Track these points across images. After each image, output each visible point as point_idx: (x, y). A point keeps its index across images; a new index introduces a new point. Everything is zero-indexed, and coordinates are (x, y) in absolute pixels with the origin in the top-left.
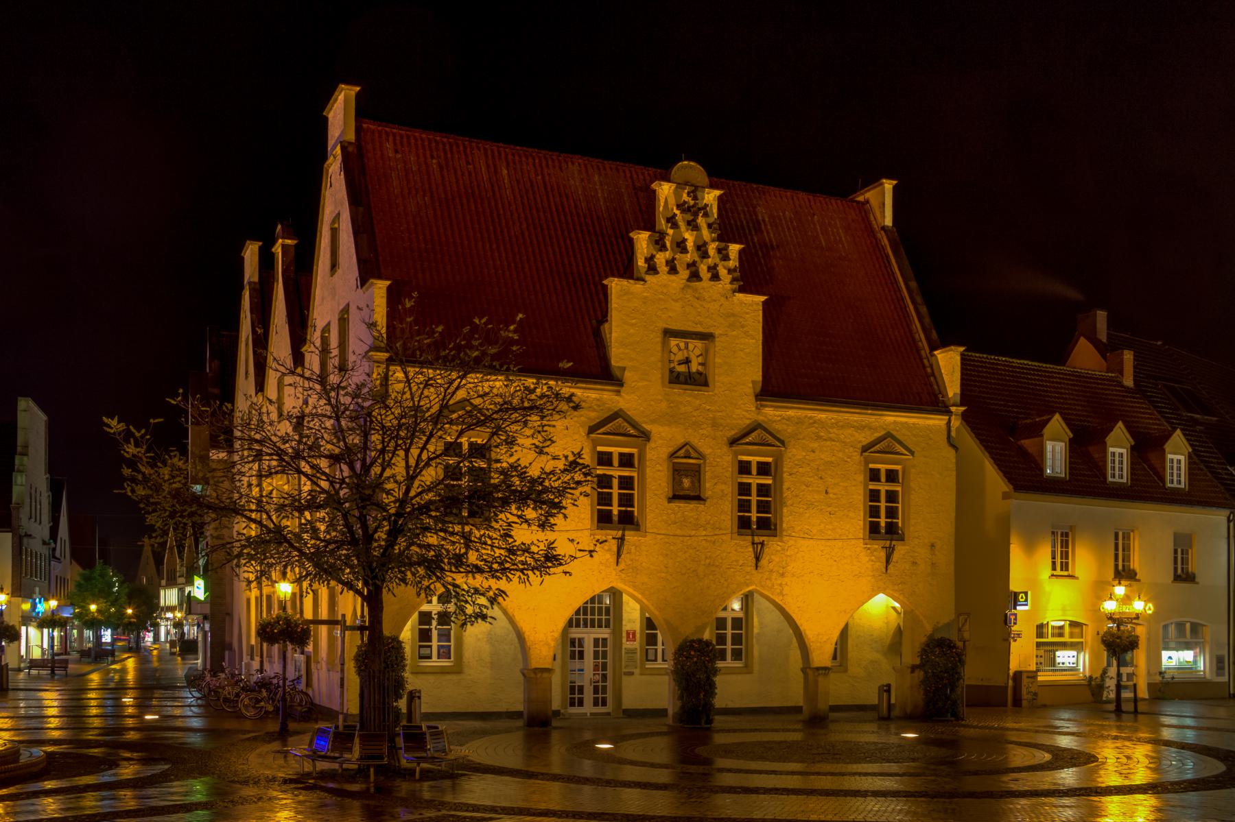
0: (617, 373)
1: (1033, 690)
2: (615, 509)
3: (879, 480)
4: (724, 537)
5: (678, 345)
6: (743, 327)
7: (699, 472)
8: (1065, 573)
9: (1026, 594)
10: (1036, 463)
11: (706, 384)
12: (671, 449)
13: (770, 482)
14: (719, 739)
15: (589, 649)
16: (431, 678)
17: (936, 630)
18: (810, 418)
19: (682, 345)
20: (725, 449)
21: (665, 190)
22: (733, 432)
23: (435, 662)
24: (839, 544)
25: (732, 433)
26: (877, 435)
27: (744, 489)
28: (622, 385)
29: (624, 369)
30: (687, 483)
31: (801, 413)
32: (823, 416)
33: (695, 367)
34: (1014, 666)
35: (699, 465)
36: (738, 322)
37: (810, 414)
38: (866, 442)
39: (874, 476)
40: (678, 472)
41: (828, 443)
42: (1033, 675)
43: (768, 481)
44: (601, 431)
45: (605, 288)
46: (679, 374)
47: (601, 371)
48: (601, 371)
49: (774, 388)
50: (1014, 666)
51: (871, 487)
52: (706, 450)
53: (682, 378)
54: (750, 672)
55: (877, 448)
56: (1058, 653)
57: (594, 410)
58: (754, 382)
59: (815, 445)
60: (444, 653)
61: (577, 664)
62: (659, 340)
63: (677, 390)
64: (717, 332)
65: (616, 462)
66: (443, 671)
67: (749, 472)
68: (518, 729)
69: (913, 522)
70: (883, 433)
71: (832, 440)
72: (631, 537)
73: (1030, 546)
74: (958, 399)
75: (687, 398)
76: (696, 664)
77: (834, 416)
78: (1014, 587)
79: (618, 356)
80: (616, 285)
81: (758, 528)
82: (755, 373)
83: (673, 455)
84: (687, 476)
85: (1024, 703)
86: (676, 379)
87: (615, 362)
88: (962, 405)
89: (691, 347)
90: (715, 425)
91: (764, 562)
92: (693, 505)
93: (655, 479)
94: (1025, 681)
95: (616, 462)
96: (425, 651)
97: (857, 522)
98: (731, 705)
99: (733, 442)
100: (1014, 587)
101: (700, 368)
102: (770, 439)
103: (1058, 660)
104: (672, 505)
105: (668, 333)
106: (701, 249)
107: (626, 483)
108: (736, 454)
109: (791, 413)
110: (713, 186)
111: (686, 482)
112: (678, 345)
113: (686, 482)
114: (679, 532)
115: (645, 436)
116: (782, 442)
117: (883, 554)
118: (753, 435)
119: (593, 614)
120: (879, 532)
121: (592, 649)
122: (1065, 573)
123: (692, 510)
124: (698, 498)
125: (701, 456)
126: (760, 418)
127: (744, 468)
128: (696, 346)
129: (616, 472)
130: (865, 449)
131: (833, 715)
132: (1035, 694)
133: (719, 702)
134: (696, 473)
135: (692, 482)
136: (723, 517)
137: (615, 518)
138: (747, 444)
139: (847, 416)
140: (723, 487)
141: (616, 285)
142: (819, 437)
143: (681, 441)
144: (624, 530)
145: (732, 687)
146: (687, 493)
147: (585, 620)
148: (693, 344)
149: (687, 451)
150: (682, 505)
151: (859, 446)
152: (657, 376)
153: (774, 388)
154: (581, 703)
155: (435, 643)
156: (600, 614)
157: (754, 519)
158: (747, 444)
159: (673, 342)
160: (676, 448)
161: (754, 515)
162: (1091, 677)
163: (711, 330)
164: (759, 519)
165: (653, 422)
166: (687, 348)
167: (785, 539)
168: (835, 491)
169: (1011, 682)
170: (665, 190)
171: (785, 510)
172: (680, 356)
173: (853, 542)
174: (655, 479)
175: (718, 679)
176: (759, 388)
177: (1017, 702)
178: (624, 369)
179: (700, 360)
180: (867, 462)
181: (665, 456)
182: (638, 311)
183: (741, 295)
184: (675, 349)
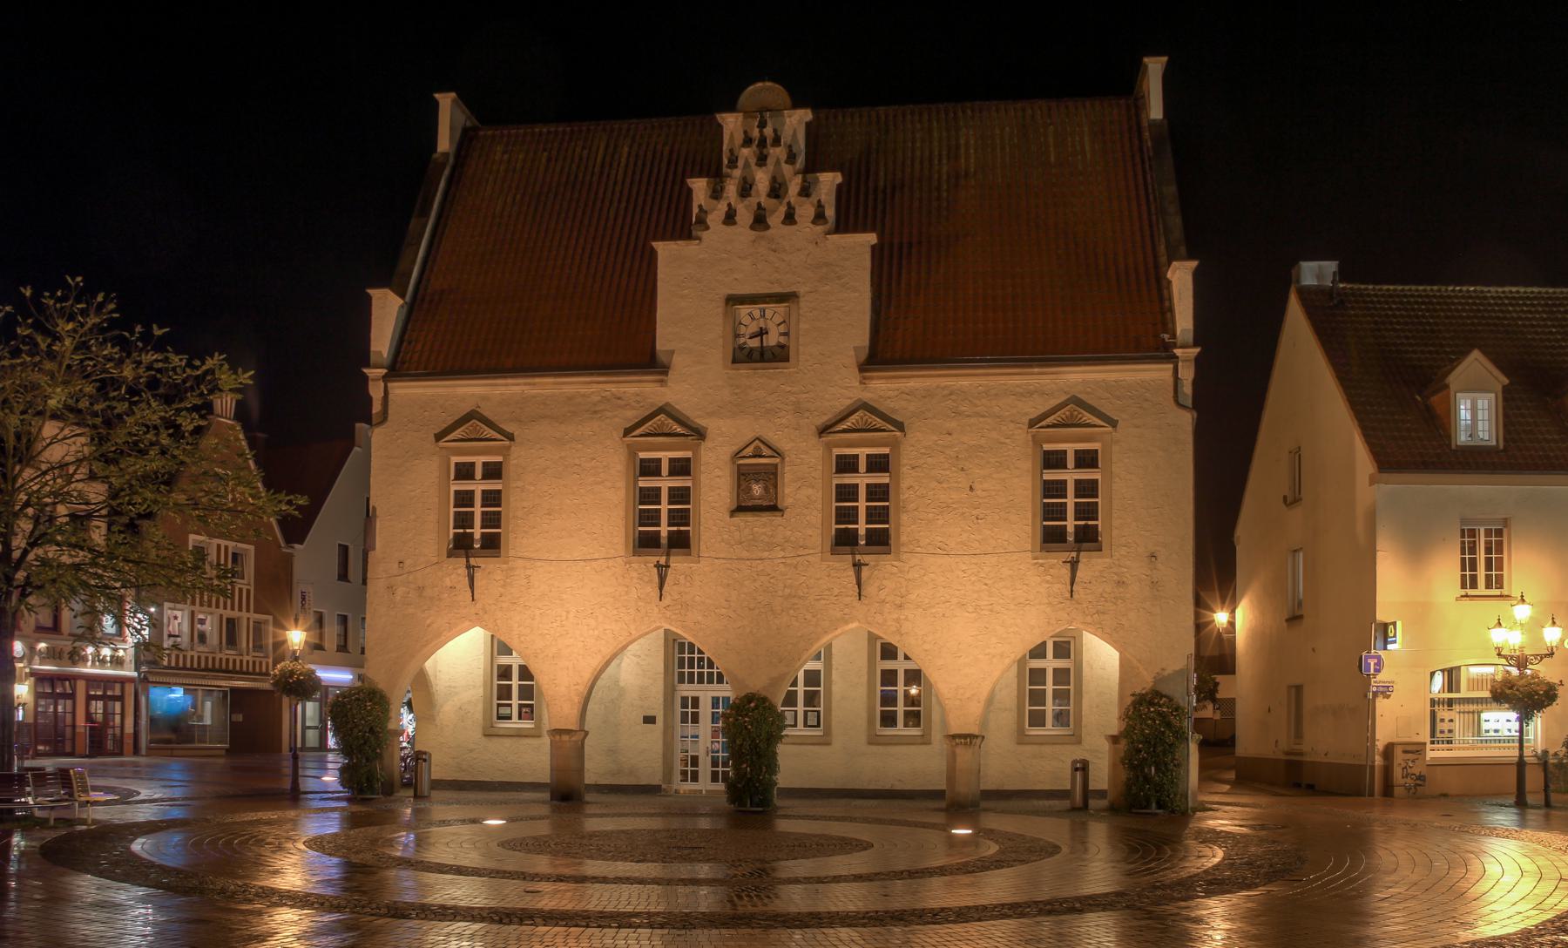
0: (662, 357)
1: (1416, 771)
2: (1071, 524)
3: (856, 471)
4: (810, 558)
5: (750, 314)
6: (839, 278)
7: (775, 474)
8: (1497, 592)
9: (1394, 624)
10: (1439, 423)
11: (787, 359)
12: (735, 448)
13: (887, 480)
14: (783, 825)
15: (705, 710)
16: (507, 742)
17: (1159, 680)
18: (944, 388)
19: (757, 314)
20: (814, 440)
21: (731, 123)
22: (825, 418)
23: (515, 724)
24: (994, 559)
25: (822, 420)
26: (1054, 402)
27: (846, 493)
28: (666, 373)
29: (673, 352)
30: (757, 489)
31: (929, 382)
32: (965, 383)
33: (772, 340)
34: (1385, 732)
35: (776, 466)
36: (834, 277)
37: (944, 382)
38: (1034, 414)
39: (1054, 460)
40: (744, 476)
41: (973, 420)
42: (1417, 749)
43: (883, 479)
44: (637, 432)
45: (653, 253)
46: (752, 349)
47: (649, 362)
48: (649, 362)
49: (881, 355)
50: (1385, 732)
51: (641, 484)
52: (783, 444)
53: (756, 355)
54: (928, 743)
55: (1050, 420)
56: (1484, 716)
57: (634, 408)
58: (856, 349)
59: (953, 425)
60: (1061, 718)
61: (690, 728)
62: (720, 310)
63: (744, 370)
64: (801, 290)
65: (1071, 461)
66: (519, 734)
67: (657, 473)
68: (544, 802)
69: (1115, 523)
70: (1064, 398)
71: (978, 415)
72: (678, 563)
73: (1417, 549)
74: (1190, 337)
75: (757, 379)
76: (752, 728)
77: (983, 381)
78: (1382, 616)
79: (666, 338)
80: (664, 249)
81: (867, 544)
82: (860, 336)
83: (737, 455)
84: (757, 481)
85: (1398, 791)
86: (744, 356)
87: (661, 345)
88: (1195, 345)
89: (769, 313)
90: (798, 410)
91: (869, 589)
92: (765, 518)
93: (714, 488)
94: (1399, 757)
95: (1071, 461)
96: (504, 711)
97: (1024, 525)
98: (899, 786)
99: (824, 430)
100: (1382, 616)
101: (782, 340)
102: (879, 423)
103: (1485, 726)
104: (736, 519)
105: (733, 300)
106: (777, 191)
107: (679, 495)
108: (829, 447)
109: (913, 384)
110: (796, 105)
111: (757, 489)
112: (750, 314)
113: (757, 489)
114: (745, 554)
115: (700, 434)
116: (900, 426)
117: (1065, 572)
118: (853, 419)
119: (691, 666)
120: (1065, 541)
121: (710, 710)
122: (1497, 592)
123: (764, 525)
124: (773, 508)
125: (778, 453)
126: (867, 396)
127: (846, 465)
128: (775, 312)
129: (1070, 476)
130: (1032, 423)
131: (983, 804)
132: (1421, 778)
133: (783, 779)
134: (770, 476)
135: (766, 489)
136: (809, 532)
137: (664, 541)
138: (844, 431)
139: (1003, 380)
140: (810, 491)
141: (664, 249)
142: (959, 414)
143: (750, 436)
144: (1079, 551)
145: (796, 762)
146: (759, 502)
147: (701, 675)
148: (770, 309)
149: (757, 448)
150: (750, 518)
151: (1026, 420)
152: (717, 356)
153: (881, 355)
154: (695, 777)
155: (515, 702)
156: (691, 666)
157: (862, 532)
158: (844, 431)
159: (744, 311)
160: (742, 445)
161: (862, 527)
162: (1545, 752)
163: (793, 289)
164: (864, 530)
165: (710, 415)
166: (763, 316)
167: (904, 557)
168: (986, 486)
169: (1378, 761)
170: (731, 123)
171: (904, 517)
172: (753, 328)
173: (1015, 556)
174: (714, 488)
175: (781, 749)
176: (864, 355)
177: (1388, 790)
178: (673, 352)
179: (782, 329)
180: (1037, 442)
181: (727, 458)
182: (692, 283)
183: (835, 237)
184: (746, 320)
